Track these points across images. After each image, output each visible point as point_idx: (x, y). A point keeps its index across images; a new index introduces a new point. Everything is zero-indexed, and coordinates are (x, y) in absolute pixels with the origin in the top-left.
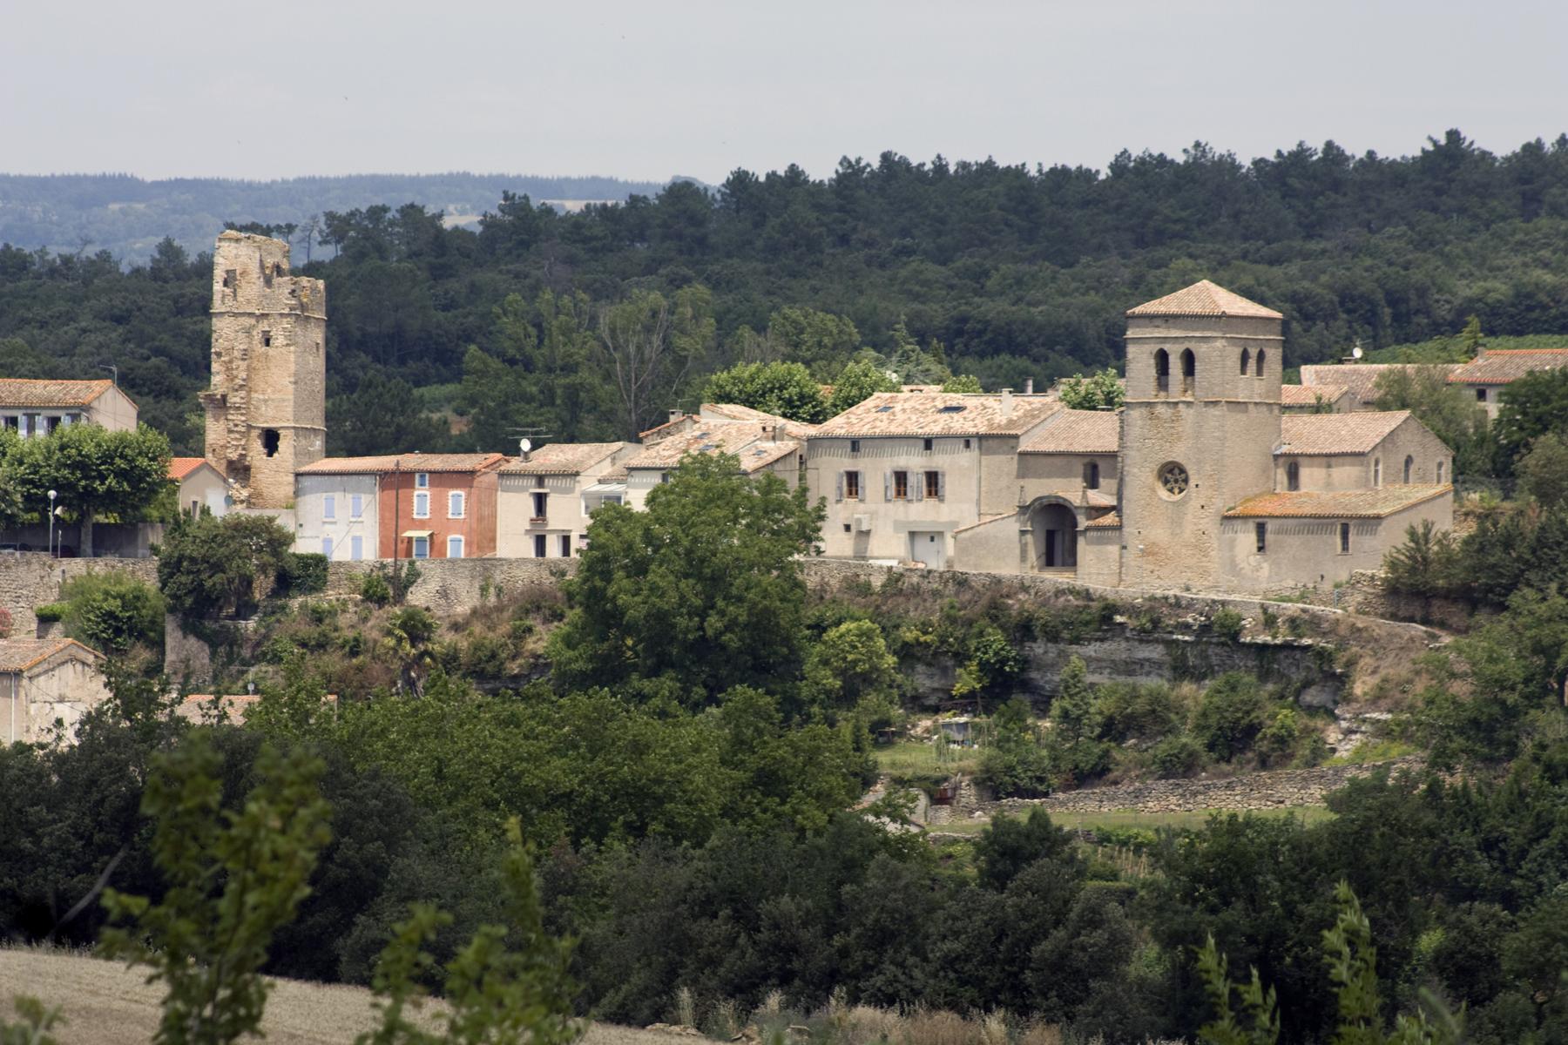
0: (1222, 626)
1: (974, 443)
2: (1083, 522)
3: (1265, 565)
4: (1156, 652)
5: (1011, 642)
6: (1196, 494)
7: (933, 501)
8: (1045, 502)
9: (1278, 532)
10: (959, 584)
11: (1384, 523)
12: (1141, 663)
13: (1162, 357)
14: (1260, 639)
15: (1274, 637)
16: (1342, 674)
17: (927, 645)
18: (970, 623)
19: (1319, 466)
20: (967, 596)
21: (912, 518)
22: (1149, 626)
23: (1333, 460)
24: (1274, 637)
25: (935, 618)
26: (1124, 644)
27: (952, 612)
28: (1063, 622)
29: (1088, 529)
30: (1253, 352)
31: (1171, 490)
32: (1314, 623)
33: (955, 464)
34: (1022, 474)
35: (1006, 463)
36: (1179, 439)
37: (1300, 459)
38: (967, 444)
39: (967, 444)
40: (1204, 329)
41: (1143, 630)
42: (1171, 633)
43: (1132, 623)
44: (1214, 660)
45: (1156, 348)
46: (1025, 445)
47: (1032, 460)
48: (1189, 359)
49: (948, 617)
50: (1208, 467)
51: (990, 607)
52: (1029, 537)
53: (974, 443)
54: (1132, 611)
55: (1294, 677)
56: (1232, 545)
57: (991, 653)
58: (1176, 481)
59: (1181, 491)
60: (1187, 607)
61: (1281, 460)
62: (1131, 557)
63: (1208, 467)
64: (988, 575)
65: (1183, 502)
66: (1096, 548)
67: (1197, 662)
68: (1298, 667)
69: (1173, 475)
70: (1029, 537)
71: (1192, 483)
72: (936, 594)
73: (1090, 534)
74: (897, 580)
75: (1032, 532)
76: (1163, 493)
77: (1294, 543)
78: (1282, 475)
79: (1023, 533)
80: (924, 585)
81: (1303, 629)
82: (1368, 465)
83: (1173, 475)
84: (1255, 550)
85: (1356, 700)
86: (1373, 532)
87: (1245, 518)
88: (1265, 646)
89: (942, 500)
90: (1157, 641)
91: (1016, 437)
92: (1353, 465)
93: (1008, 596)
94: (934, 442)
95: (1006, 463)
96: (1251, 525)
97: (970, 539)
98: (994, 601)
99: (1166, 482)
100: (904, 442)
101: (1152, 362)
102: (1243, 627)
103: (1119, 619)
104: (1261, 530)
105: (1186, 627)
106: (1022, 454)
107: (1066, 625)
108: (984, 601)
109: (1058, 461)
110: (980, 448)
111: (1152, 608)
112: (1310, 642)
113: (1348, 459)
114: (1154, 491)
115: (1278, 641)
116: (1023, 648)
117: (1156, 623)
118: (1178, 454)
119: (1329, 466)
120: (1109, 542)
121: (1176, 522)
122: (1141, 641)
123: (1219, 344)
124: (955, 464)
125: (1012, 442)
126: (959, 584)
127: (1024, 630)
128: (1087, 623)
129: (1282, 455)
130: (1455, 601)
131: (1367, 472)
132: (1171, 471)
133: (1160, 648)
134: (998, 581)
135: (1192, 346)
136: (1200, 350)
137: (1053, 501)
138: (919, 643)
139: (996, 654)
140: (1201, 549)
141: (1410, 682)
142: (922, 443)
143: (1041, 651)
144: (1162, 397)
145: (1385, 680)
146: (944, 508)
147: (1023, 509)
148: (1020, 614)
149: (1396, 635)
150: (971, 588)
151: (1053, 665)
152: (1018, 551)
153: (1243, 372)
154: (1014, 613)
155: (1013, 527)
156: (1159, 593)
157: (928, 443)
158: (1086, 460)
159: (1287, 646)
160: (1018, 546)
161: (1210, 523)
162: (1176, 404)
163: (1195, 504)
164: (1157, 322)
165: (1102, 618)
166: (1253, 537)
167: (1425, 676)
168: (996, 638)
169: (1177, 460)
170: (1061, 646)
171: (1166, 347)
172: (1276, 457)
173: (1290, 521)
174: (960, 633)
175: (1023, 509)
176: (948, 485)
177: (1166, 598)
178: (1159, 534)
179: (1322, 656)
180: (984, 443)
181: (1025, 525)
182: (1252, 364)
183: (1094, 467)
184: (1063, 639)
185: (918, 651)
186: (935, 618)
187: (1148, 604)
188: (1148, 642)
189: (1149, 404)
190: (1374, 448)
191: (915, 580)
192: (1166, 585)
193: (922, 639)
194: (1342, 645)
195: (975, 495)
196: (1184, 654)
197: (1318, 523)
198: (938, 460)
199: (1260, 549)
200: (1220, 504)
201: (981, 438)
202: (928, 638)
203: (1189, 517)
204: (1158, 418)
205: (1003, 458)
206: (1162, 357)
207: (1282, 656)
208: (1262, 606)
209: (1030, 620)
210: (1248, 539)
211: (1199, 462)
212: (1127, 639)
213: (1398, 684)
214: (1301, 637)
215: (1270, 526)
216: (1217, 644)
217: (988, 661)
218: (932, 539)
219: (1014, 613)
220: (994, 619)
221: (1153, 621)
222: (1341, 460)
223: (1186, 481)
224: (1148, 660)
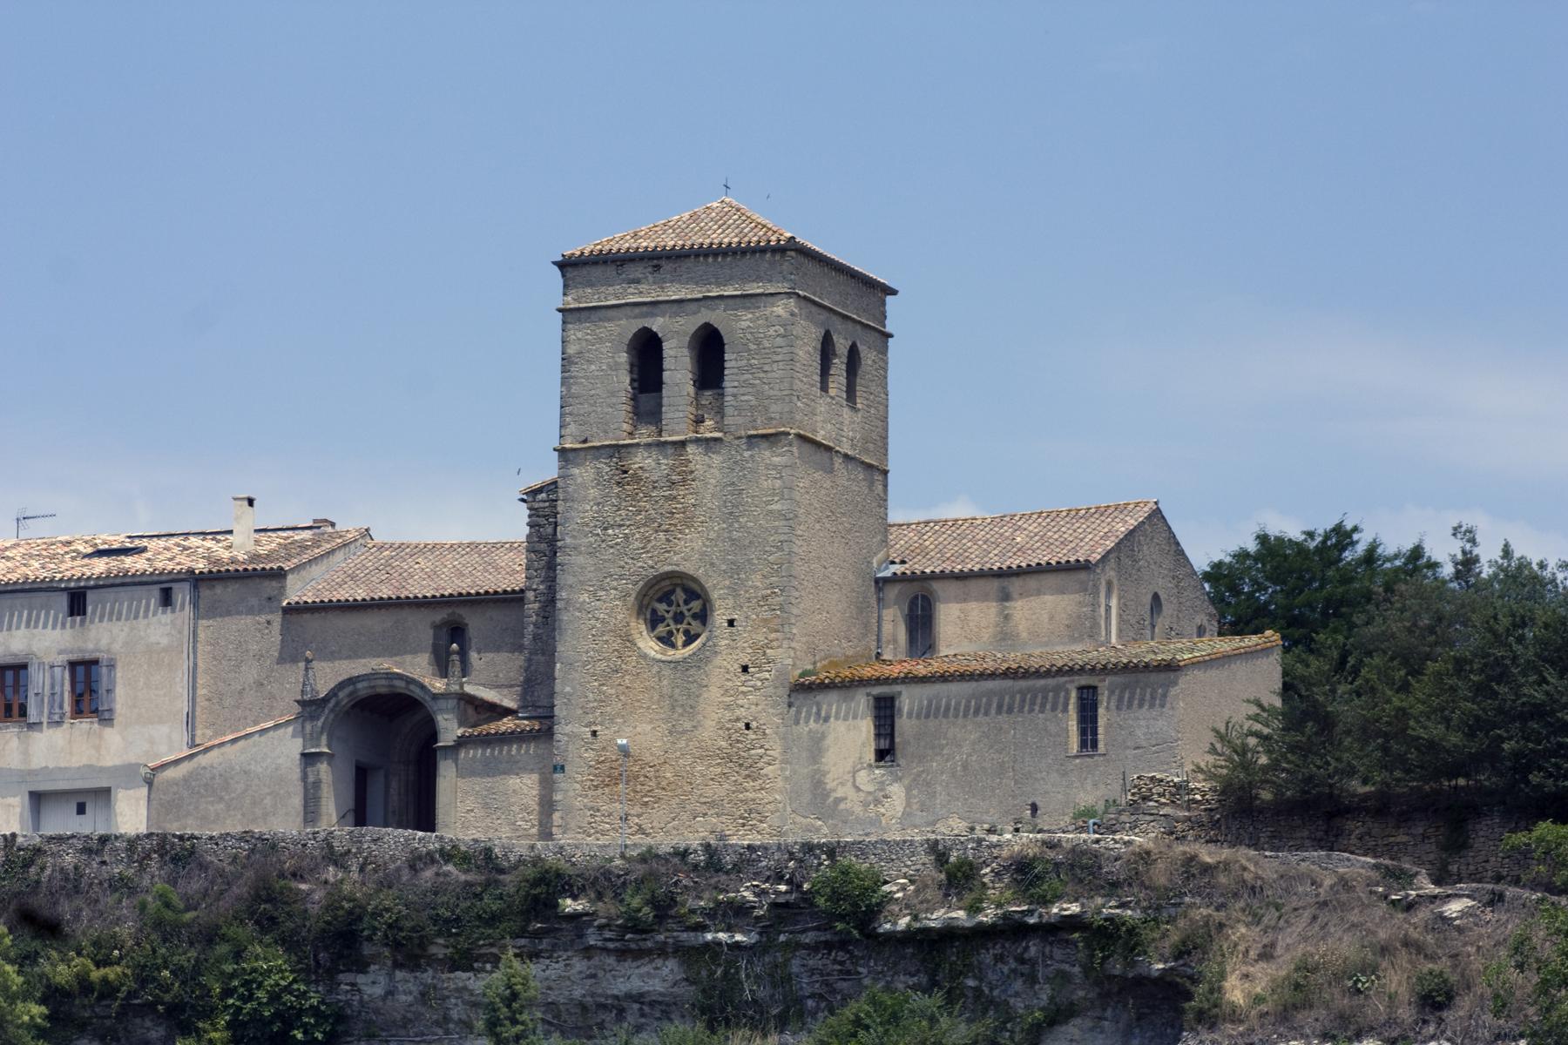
0: (836, 896)
1: (182, 594)
2: (450, 729)
3: (897, 791)
4: (657, 977)
5: (308, 972)
6: (726, 648)
7: (85, 725)
8: (363, 689)
9: (929, 712)
10: (175, 859)
11: (1185, 681)
12: (618, 1007)
13: (647, 351)
14: (936, 918)
15: (974, 909)
16: (1163, 980)
17: (108, 990)
18: (210, 936)
19: (984, 598)
20: (196, 885)
21: (37, 762)
22: (647, 913)
23: (1015, 585)
24: (974, 909)
25: (126, 931)
26: (579, 965)
27: (169, 915)
28: (435, 919)
29: (462, 742)
30: (841, 345)
31: (667, 640)
32: (1083, 869)
33: (138, 642)
34: (290, 654)
35: (255, 633)
36: (688, 522)
37: (936, 586)
38: (167, 599)
39: (167, 599)
40: (745, 280)
41: (635, 926)
42: (702, 928)
43: (607, 908)
44: (806, 985)
45: (629, 327)
46: (298, 591)
47: (313, 623)
48: (710, 350)
49: (159, 924)
50: (756, 580)
51: (257, 898)
52: (323, 767)
53: (182, 594)
54: (601, 882)
55: (1018, 1005)
56: (816, 747)
57: (261, 995)
58: (679, 618)
59: (690, 638)
60: (737, 868)
61: (892, 592)
62: (570, 790)
63: (756, 580)
64: (245, 836)
65: (699, 661)
66: (479, 784)
67: (763, 993)
68: (1032, 980)
69: (674, 603)
70: (323, 767)
71: (719, 618)
72: (121, 885)
73: (468, 754)
74: (27, 864)
75: (330, 757)
76: (649, 645)
77: (965, 739)
78: (894, 624)
79: (308, 759)
80: (92, 868)
81: (1051, 884)
82: (1096, 593)
83: (674, 603)
84: (870, 756)
85: (1235, 1016)
86: (1158, 700)
87: (848, 686)
88: (949, 934)
89: (106, 718)
90: (662, 952)
91: (280, 574)
92: (1061, 591)
93: (297, 875)
94: (91, 597)
95: (255, 633)
96: (862, 701)
97: (185, 780)
98: (265, 889)
99: (654, 621)
100: (20, 599)
101: (624, 358)
102: (889, 898)
103: (569, 905)
104: (885, 712)
105: (737, 913)
106: (291, 610)
107: (446, 925)
108: (240, 890)
109: (372, 621)
110: (195, 604)
111: (652, 876)
112: (1075, 908)
113: (1050, 580)
114: (628, 640)
115: (988, 916)
116: (333, 987)
117: (664, 907)
118: (689, 554)
119: (1005, 597)
120: (513, 768)
121: (682, 704)
122: (623, 954)
123: (780, 309)
124: (138, 642)
125: (270, 587)
126: (175, 859)
127: (342, 941)
128: (493, 919)
129: (895, 579)
130: (1404, 819)
131: (1095, 606)
132: (666, 598)
133: (670, 969)
134: (269, 846)
135: (716, 317)
136: (736, 325)
137: (382, 687)
138: (85, 985)
139: (275, 997)
140: (739, 759)
141: (1370, 969)
142: (63, 601)
143: (378, 991)
144: (645, 435)
145: (1305, 967)
146: (112, 736)
147: (310, 707)
148: (331, 907)
149: (1300, 878)
150: (204, 867)
151: (406, 1023)
152: (297, 801)
153: (824, 388)
154: (314, 909)
155: (289, 747)
156: (665, 843)
157: (77, 599)
158: (440, 616)
159: (1012, 930)
160: (298, 788)
161: (760, 703)
162: (683, 444)
163: (726, 661)
164: (636, 271)
165: (534, 903)
166: (864, 729)
167: (1403, 957)
168: (271, 964)
169: (688, 568)
170: (428, 976)
171: (657, 324)
172: (881, 583)
173: (954, 688)
174: (187, 956)
175: (310, 707)
176: (123, 693)
177: (683, 854)
178: (640, 733)
179: (1105, 935)
180: (205, 592)
181: (313, 739)
182: (839, 366)
183: (456, 632)
184: (432, 961)
185: (82, 1008)
186: (126, 931)
187: (640, 870)
188: (640, 954)
189: (617, 450)
190: (1105, 558)
191: (69, 860)
192: (675, 829)
193: (96, 975)
194: (1162, 905)
195: (183, 706)
196: (731, 980)
197: (1017, 685)
198: (102, 635)
199: (882, 755)
200: (790, 659)
201: (197, 580)
202: (112, 973)
203: (714, 693)
204: (637, 479)
205: (246, 621)
206: (647, 351)
207: (987, 957)
208: (933, 847)
209: (355, 915)
210: (851, 733)
211: (735, 570)
212: (588, 952)
213: (1338, 977)
214: (1045, 902)
215: (908, 699)
216: (814, 948)
217: (255, 1015)
218: (81, 810)
219: (314, 909)
220: (267, 924)
221: (652, 906)
222: (1032, 582)
223: (703, 617)
224: (638, 998)
